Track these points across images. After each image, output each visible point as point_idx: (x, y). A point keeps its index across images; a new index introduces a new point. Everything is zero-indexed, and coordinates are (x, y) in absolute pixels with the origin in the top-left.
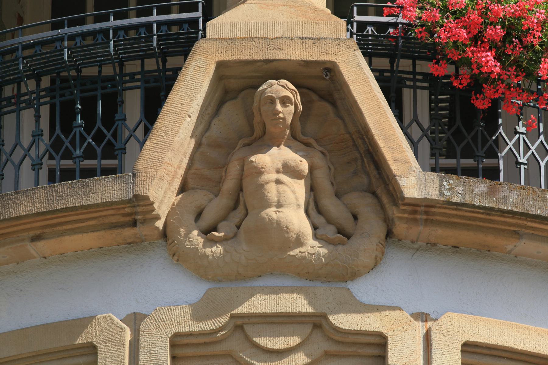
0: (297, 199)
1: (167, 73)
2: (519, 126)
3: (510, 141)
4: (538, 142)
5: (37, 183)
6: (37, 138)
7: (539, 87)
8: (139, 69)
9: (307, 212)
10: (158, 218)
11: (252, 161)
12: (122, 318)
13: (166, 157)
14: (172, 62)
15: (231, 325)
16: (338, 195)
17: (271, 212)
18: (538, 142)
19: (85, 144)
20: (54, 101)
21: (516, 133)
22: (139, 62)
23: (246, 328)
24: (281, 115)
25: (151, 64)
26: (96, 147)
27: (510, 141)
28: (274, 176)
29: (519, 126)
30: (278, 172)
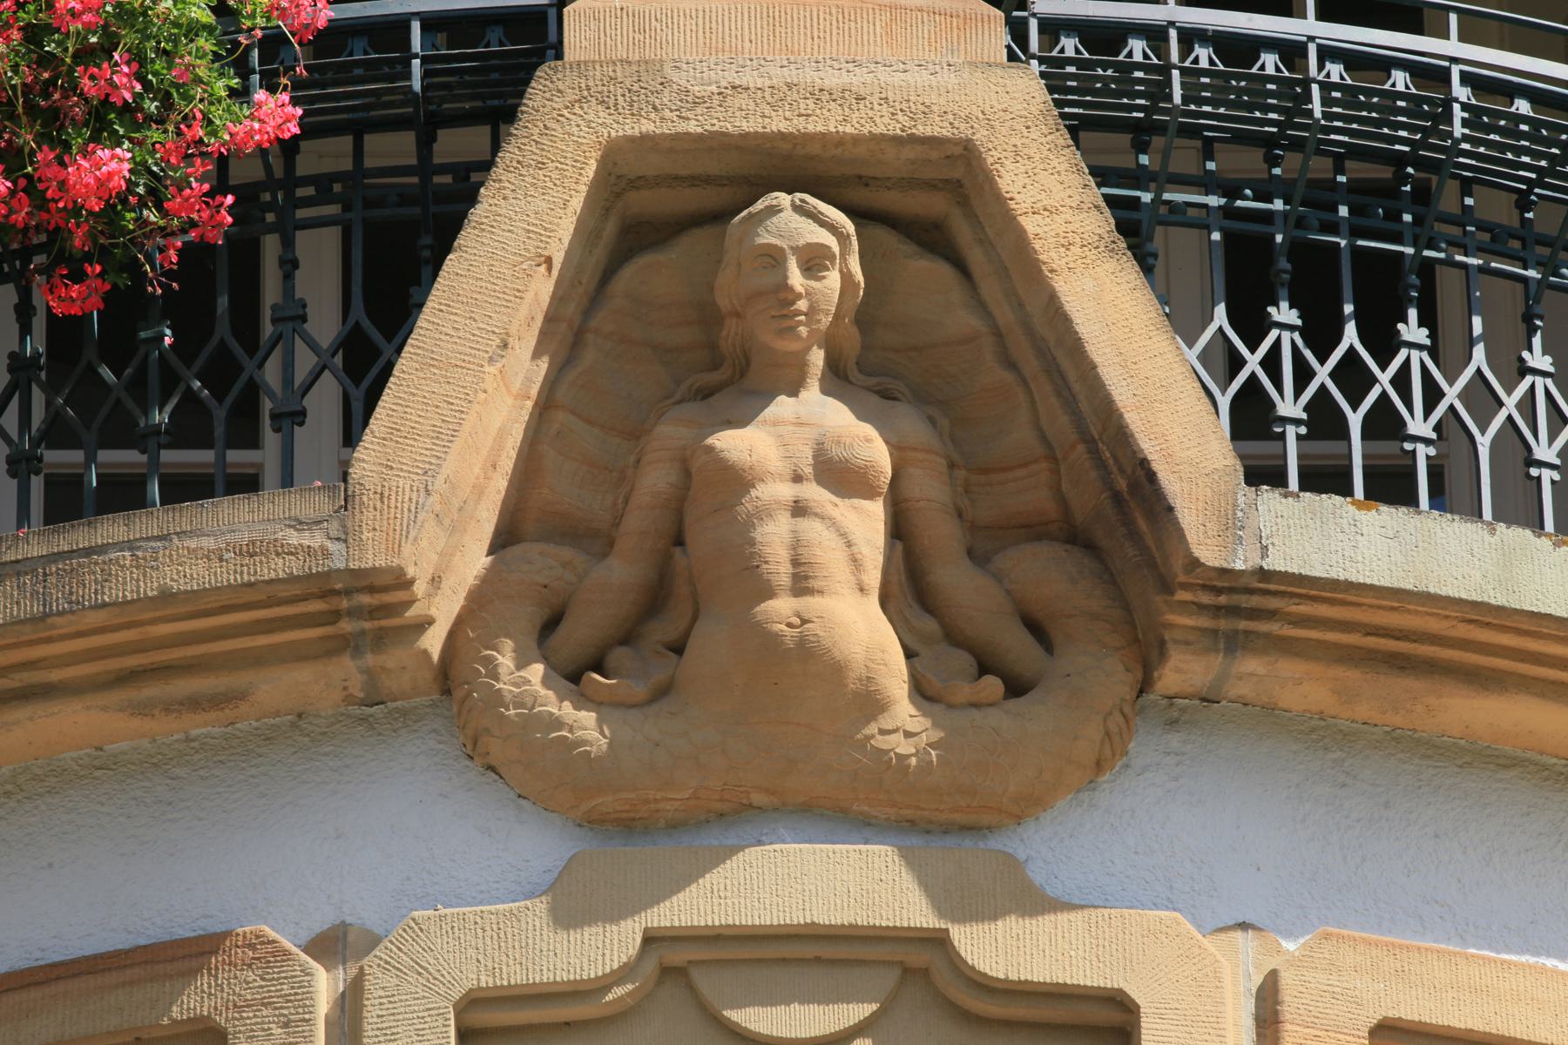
0: (856, 562)
1: (437, 179)
2: (1531, 351)
3: (1509, 393)
4: (1469, 372)
5: (23, 516)
6: (287, 328)
7: (1469, 201)
8: (347, 165)
9: (884, 602)
10: (425, 623)
11: (711, 449)
12: (303, 942)
13: (455, 430)
14: (454, 144)
15: (650, 967)
16: (978, 557)
17: (780, 609)
18: (1469, 372)
19: (106, 409)
20: (348, 215)
21: (1524, 370)
22: (346, 142)
23: (700, 978)
24: (802, 305)
25: (392, 149)
26: (212, 403)
27: (1509, 393)
28: (785, 491)
29: (1531, 351)
30: (797, 478)
